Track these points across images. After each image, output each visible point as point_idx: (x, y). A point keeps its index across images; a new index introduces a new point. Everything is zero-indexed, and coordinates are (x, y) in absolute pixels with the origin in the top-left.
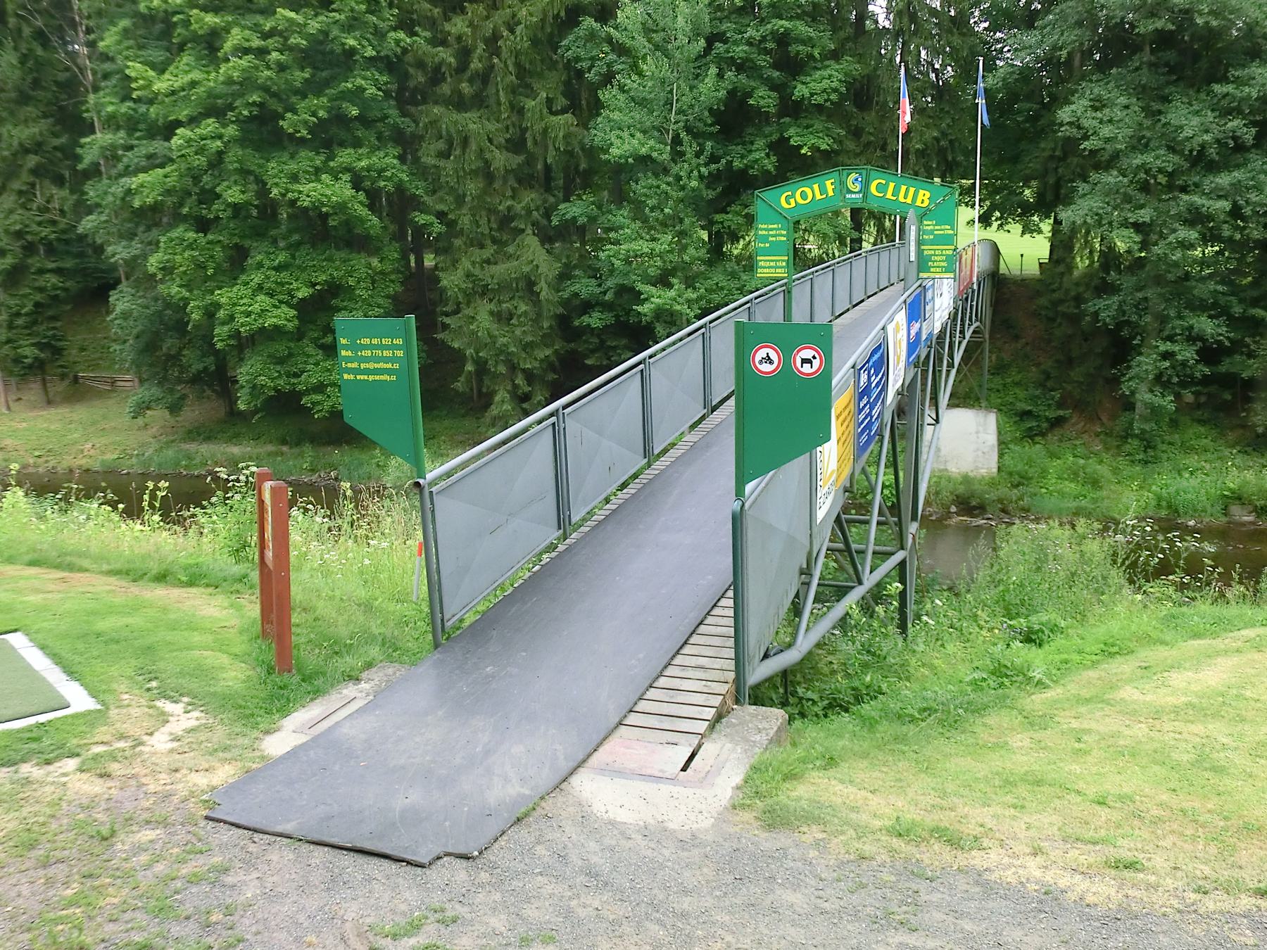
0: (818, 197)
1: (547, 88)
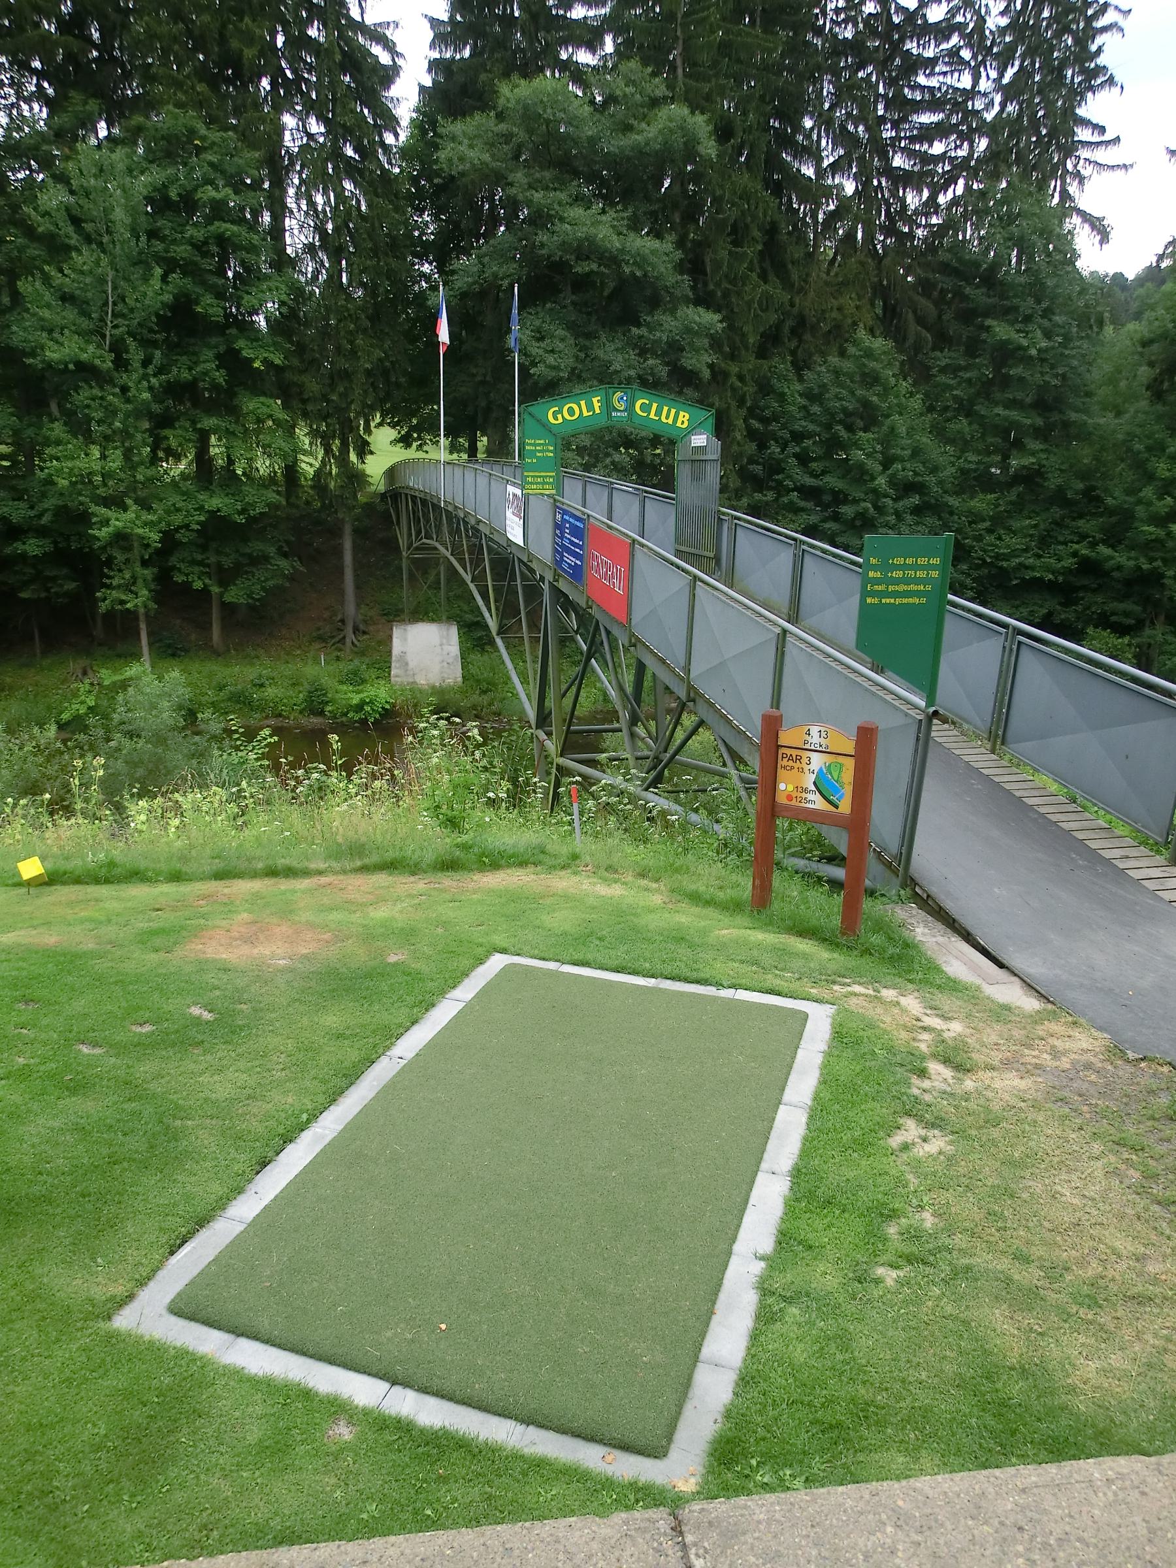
0: (585, 414)
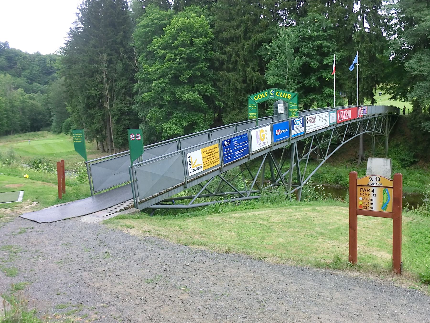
0: (263, 97)
1: (254, 63)
